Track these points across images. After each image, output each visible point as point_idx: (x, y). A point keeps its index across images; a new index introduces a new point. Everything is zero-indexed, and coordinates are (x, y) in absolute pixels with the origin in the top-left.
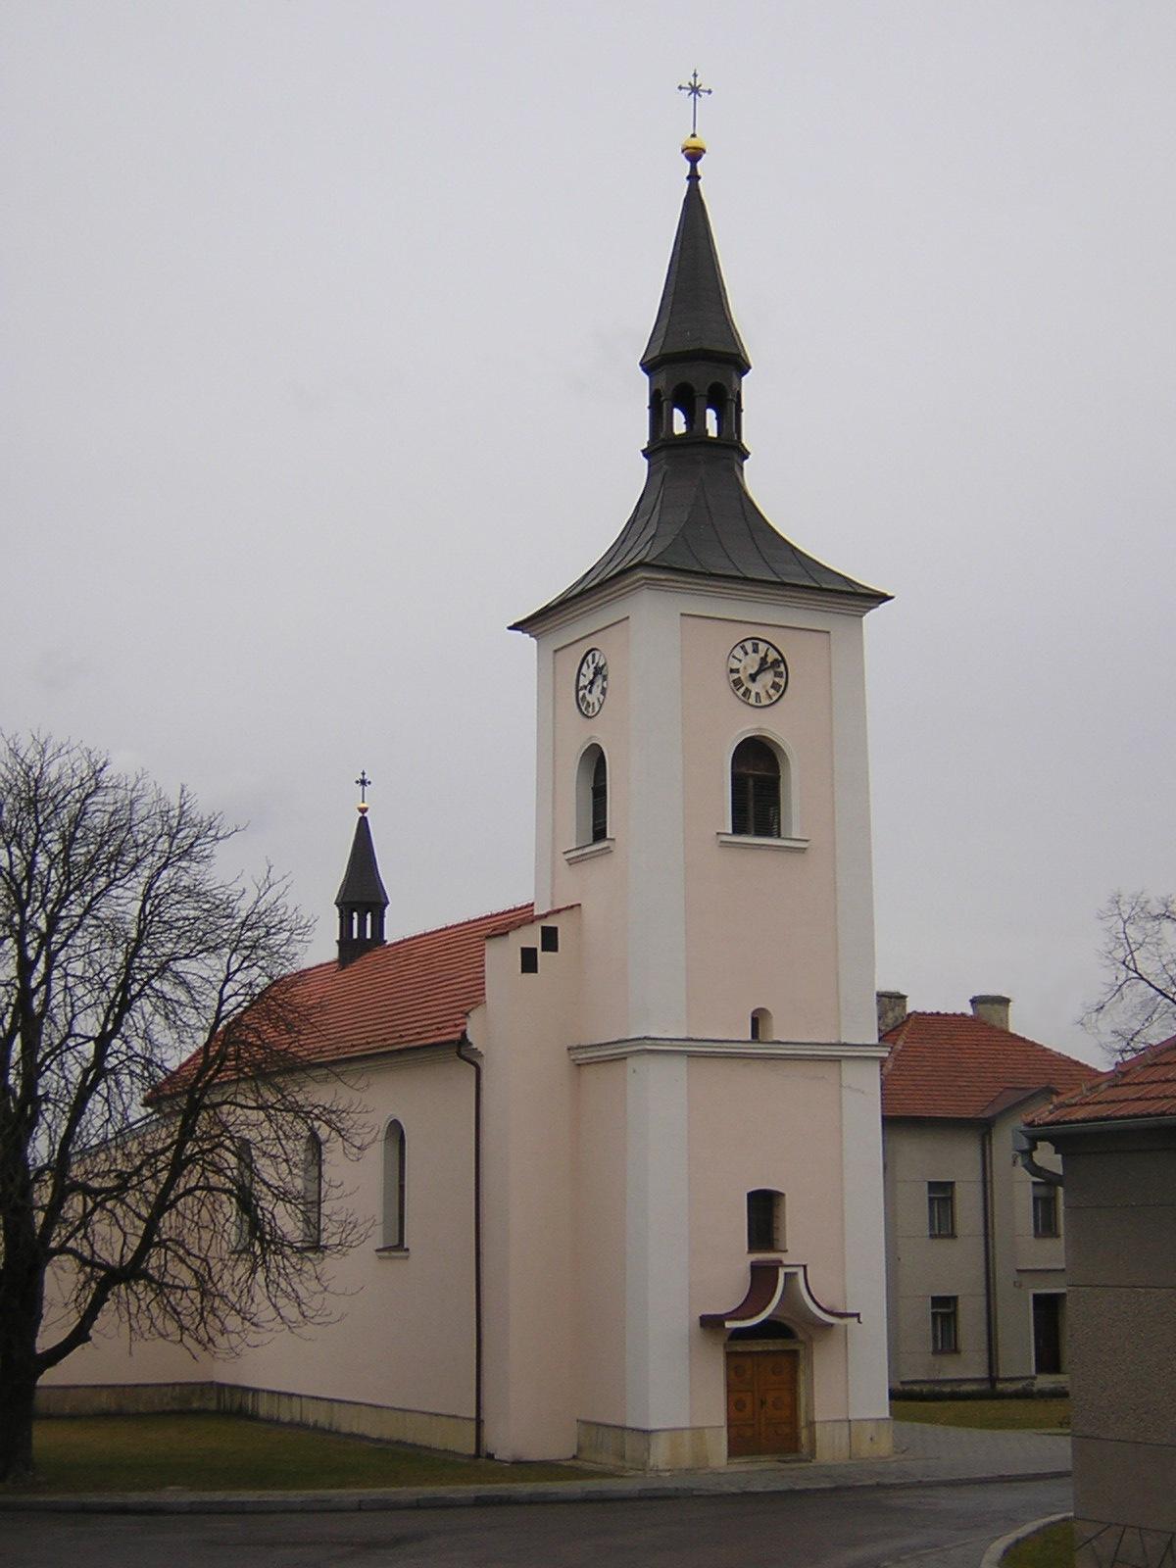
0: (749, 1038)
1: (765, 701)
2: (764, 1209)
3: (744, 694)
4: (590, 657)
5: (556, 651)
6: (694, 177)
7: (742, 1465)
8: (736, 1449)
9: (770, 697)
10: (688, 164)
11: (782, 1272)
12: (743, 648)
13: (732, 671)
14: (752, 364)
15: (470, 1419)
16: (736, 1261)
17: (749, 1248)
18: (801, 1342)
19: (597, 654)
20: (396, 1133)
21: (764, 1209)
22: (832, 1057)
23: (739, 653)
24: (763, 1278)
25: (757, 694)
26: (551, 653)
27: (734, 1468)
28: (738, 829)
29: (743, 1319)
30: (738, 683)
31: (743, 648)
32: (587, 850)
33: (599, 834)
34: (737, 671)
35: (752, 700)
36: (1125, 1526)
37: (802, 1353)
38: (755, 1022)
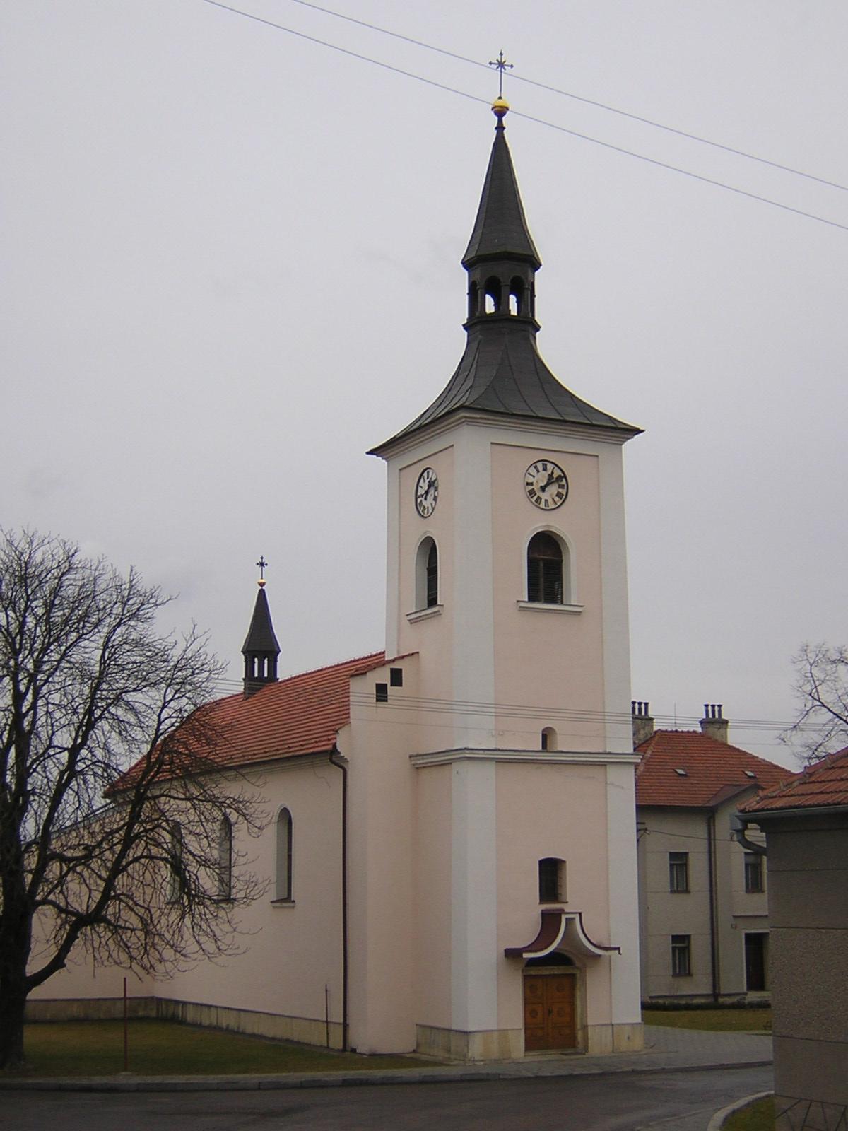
0: (540, 749)
1: (552, 506)
2: (551, 872)
3: (536, 501)
4: (425, 474)
5: (401, 470)
6: (500, 128)
7: (535, 1057)
8: (531, 1045)
9: (555, 503)
10: (496, 118)
11: (564, 917)
12: (536, 467)
13: (528, 484)
14: (542, 263)
15: (339, 1024)
16: (531, 909)
17: (541, 900)
18: (578, 968)
19: (431, 471)
20: (286, 817)
21: (551, 872)
22: (600, 762)
23: (533, 471)
24: (550, 921)
25: (546, 500)
26: (398, 471)
27: (529, 1059)
28: (532, 598)
29: (536, 951)
30: (532, 493)
31: (536, 467)
32: (423, 613)
33: (432, 601)
34: (531, 484)
35: (542, 505)
36: (811, 1101)
37: (578, 976)
38: (545, 737)
